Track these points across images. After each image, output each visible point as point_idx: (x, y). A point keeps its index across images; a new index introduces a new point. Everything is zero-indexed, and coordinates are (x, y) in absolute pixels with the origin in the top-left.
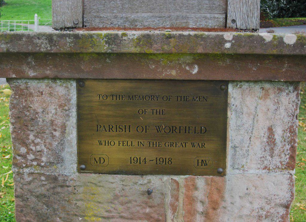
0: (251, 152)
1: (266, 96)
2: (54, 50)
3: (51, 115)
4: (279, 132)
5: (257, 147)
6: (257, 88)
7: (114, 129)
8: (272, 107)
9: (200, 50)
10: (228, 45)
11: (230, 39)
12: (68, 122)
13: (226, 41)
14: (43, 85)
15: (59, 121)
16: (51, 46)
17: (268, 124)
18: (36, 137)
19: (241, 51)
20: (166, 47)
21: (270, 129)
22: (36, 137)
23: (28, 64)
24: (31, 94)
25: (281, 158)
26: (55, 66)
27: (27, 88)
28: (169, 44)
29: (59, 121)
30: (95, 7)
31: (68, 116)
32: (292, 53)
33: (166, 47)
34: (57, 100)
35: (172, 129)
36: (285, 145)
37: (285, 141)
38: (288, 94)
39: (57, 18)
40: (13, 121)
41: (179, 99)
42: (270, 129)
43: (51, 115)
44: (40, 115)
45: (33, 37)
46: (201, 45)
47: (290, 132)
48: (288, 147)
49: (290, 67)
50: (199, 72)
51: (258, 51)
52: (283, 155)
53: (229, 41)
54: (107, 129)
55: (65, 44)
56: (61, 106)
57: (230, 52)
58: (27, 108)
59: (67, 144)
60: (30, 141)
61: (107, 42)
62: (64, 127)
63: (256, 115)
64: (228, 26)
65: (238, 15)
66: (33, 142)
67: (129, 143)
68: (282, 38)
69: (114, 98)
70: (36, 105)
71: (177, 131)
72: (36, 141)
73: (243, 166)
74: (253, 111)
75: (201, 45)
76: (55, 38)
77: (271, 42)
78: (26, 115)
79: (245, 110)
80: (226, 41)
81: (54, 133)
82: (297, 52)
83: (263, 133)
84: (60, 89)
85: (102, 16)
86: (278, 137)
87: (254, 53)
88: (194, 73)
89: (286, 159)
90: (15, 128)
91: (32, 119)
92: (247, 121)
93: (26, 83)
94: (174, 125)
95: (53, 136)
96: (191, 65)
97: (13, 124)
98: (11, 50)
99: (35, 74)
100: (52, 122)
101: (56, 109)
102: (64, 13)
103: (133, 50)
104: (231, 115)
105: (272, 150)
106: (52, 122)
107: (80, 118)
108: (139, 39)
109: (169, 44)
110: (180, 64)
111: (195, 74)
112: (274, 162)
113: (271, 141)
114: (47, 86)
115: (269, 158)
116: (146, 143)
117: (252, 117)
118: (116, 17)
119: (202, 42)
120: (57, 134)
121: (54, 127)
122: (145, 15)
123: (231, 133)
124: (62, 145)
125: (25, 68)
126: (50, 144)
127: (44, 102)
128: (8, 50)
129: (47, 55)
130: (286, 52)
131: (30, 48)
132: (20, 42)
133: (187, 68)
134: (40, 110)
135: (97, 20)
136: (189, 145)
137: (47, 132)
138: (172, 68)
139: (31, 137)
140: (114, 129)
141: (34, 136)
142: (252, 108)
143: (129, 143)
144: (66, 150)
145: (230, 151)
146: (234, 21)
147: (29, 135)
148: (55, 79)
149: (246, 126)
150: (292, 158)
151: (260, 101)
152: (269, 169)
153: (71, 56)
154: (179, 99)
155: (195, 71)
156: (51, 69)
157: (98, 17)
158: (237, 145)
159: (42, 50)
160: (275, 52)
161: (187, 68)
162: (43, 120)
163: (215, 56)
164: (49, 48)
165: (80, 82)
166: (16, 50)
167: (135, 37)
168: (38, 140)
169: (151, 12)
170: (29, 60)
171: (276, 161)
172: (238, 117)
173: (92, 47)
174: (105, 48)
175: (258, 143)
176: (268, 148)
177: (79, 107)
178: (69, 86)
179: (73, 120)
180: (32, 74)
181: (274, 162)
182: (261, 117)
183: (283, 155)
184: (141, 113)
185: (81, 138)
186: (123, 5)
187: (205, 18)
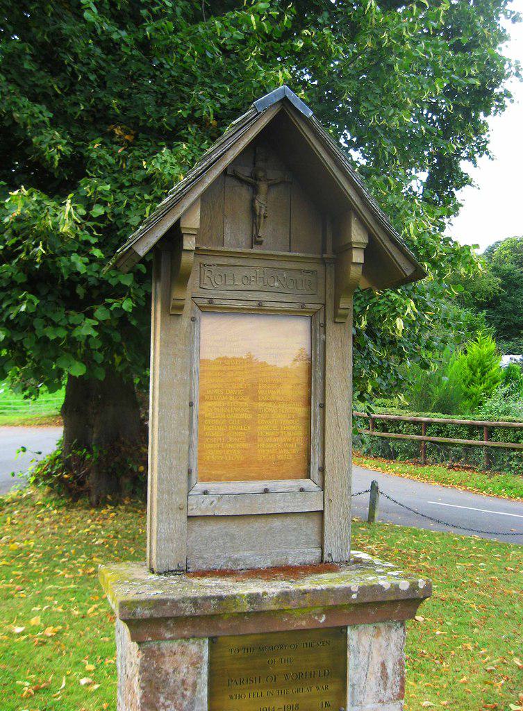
0: (368, 688)
1: (378, 634)
2: (199, 612)
3: (182, 674)
4: (390, 666)
5: (373, 682)
6: (370, 627)
7: (245, 682)
8: (384, 644)
9: (331, 602)
10: (354, 596)
11: (356, 590)
12: (199, 680)
13: (353, 593)
14: (175, 646)
15: (190, 681)
16: (195, 610)
17: (381, 659)
18: (166, 699)
19: (365, 600)
20: (302, 602)
21: (383, 665)
22: (166, 699)
23: (166, 626)
24: (163, 655)
25: (392, 690)
26: (193, 626)
27: (159, 649)
28: (304, 599)
29: (190, 681)
30: (196, 548)
31: (200, 673)
32: (406, 598)
33: (302, 602)
34: (189, 659)
35: (299, 676)
36: (395, 677)
37: (395, 674)
38: (396, 630)
39: (160, 562)
40: (143, 685)
41: (305, 645)
42: (383, 665)
43: (182, 674)
44: (171, 675)
45: (177, 602)
46: (332, 598)
47: (400, 664)
48: (398, 679)
49: (402, 608)
50: (326, 620)
51: (379, 599)
52: (394, 687)
53: (356, 592)
54: (238, 682)
55: (209, 607)
56: (193, 664)
57: (357, 602)
58: (158, 669)
59: (197, 703)
60: (160, 704)
61: (249, 602)
62: (195, 685)
63: (370, 653)
64: (324, 560)
65: (333, 549)
66: (163, 704)
67: (259, 694)
68: (398, 585)
69: (246, 650)
70: (168, 666)
71: (304, 676)
72: (166, 704)
73: (361, 703)
74: (367, 649)
75: (332, 598)
76: (199, 601)
77: (390, 589)
78: (157, 678)
79: (361, 649)
80: (353, 593)
81: (185, 693)
82: (410, 596)
83: (376, 668)
84: (193, 648)
85: (205, 556)
86: (389, 671)
87: (377, 600)
88: (321, 622)
89: (397, 690)
90: (145, 692)
91: (164, 681)
92: (363, 658)
93: (159, 644)
94: (300, 671)
95: (184, 696)
96: (320, 615)
97: (142, 688)
98: (155, 616)
99: (172, 635)
100: (183, 682)
101: (188, 668)
102: (168, 556)
103: (273, 607)
104: (350, 656)
105: (385, 683)
106: (183, 682)
107: (211, 674)
108: (278, 597)
109: (304, 599)
110: (310, 615)
111: (323, 623)
112: (387, 695)
113: (384, 675)
114: (179, 645)
115: (382, 691)
116: (275, 692)
117: (367, 655)
118: (219, 557)
119: (333, 595)
120: (188, 693)
121: (185, 687)
122: (247, 553)
123: (350, 673)
124: (191, 703)
125: (162, 630)
126: (181, 705)
127: (176, 661)
128: (151, 616)
129: (193, 617)
130: (401, 597)
131: (174, 612)
132: (164, 607)
133: (316, 618)
134: (171, 670)
135: (201, 561)
136: (314, 689)
137: (179, 692)
138: (302, 619)
139: (162, 700)
140: (245, 682)
141: (164, 698)
142: (367, 646)
143: (259, 694)
144: (196, 708)
145: (349, 689)
146: (330, 555)
147: (159, 698)
148: (186, 638)
149: (362, 664)
150: (402, 688)
151: (373, 639)
152: (383, 702)
153: (211, 617)
154: (305, 645)
155: (323, 620)
156: (188, 630)
157: (202, 558)
158: (355, 683)
159: (186, 614)
160: (392, 598)
161: (316, 618)
162: (174, 679)
163: (342, 607)
164: (193, 612)
165: (213, 642)
166: (160, 615)
167: (275, 595)
168: (169, 702)
169: (252, 550)
170: (169, 622)
171: (389, 693)
172: (355, 657)
173: (235, 607)
174: (247, 607)
175: (373, 679)
176: (382, 682)
177: (211, 663)
178: (202, 644)
179: (205, 676)
180: (168, 635)
181: (387, 695)
182: (375, 655)
183: (394, 687)
184: (270, 662)
185: (212, 696)
186: (224, 544)
187: (304, 553)
